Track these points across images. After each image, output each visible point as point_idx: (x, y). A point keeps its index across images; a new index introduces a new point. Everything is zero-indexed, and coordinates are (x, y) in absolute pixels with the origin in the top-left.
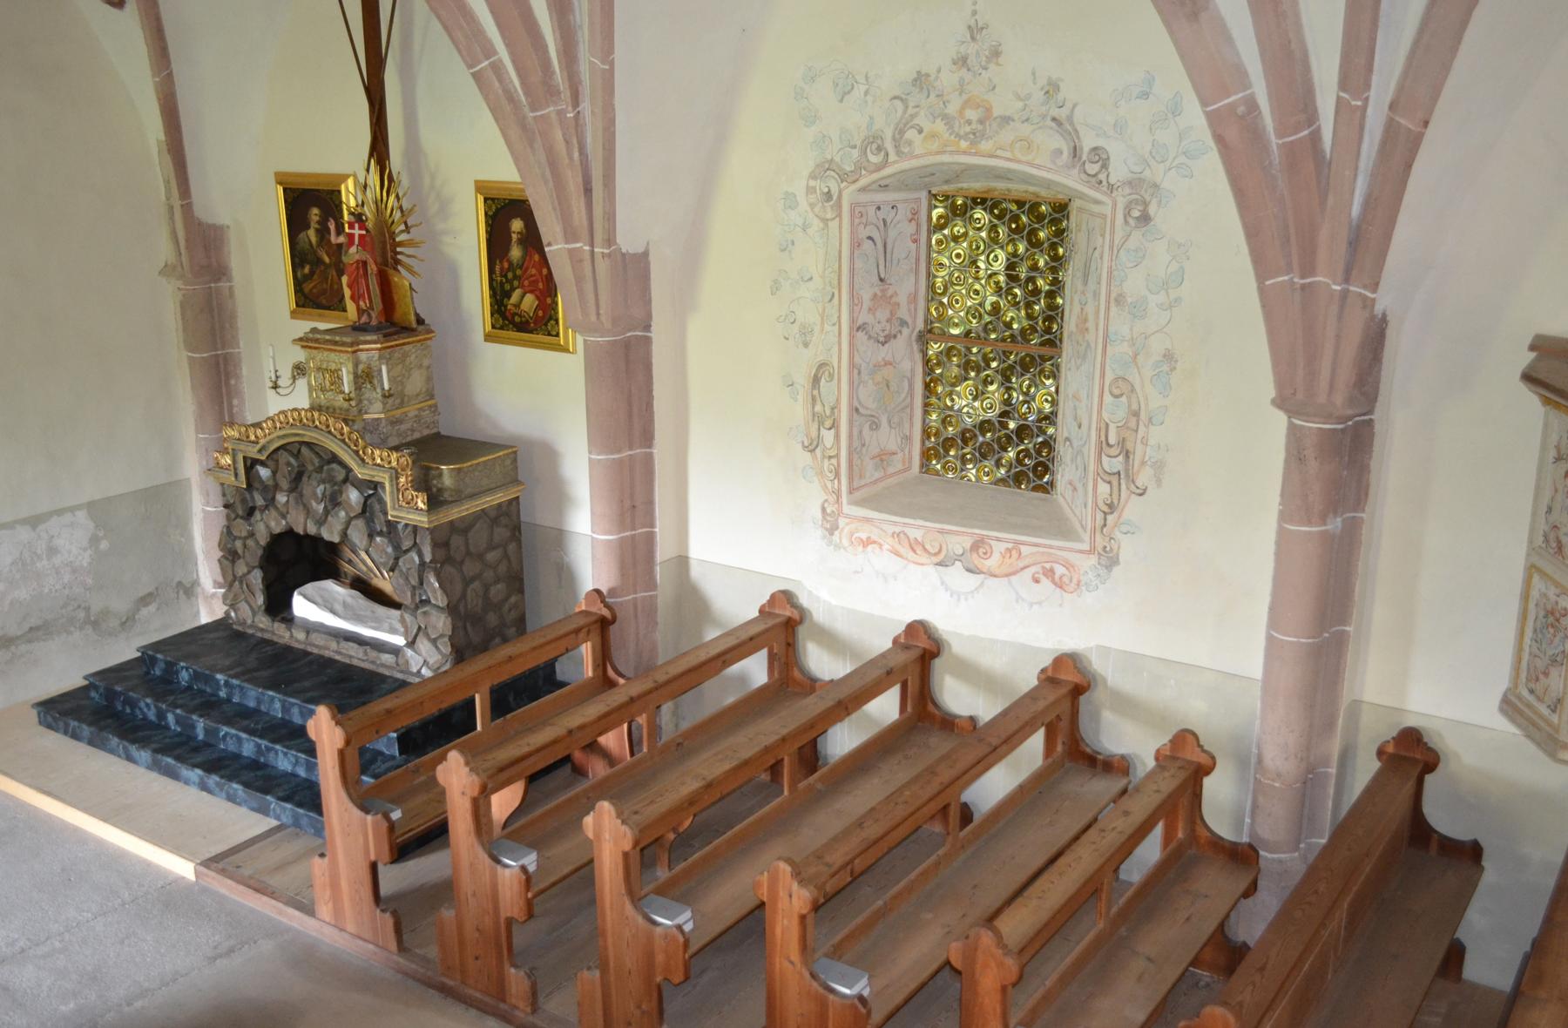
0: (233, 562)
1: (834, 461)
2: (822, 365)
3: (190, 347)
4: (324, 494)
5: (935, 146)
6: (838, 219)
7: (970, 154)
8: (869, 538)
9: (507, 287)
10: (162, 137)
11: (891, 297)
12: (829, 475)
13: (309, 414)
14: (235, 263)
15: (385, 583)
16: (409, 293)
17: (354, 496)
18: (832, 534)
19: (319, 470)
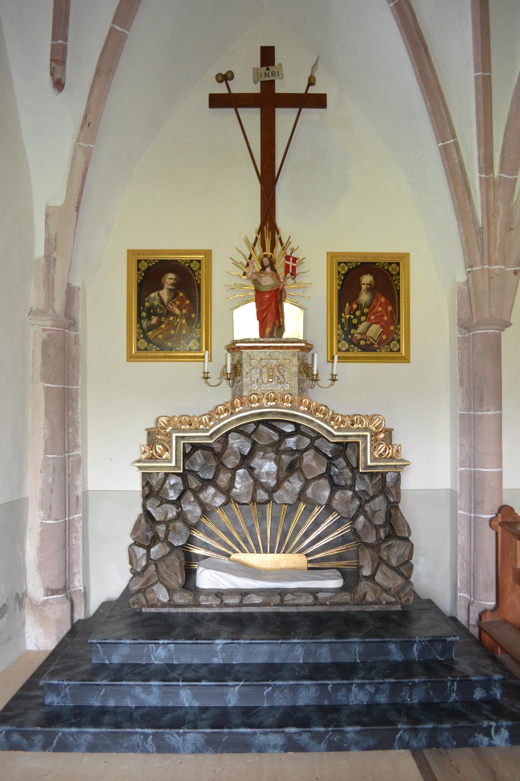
3: (45, 378)
9: (355, 321)
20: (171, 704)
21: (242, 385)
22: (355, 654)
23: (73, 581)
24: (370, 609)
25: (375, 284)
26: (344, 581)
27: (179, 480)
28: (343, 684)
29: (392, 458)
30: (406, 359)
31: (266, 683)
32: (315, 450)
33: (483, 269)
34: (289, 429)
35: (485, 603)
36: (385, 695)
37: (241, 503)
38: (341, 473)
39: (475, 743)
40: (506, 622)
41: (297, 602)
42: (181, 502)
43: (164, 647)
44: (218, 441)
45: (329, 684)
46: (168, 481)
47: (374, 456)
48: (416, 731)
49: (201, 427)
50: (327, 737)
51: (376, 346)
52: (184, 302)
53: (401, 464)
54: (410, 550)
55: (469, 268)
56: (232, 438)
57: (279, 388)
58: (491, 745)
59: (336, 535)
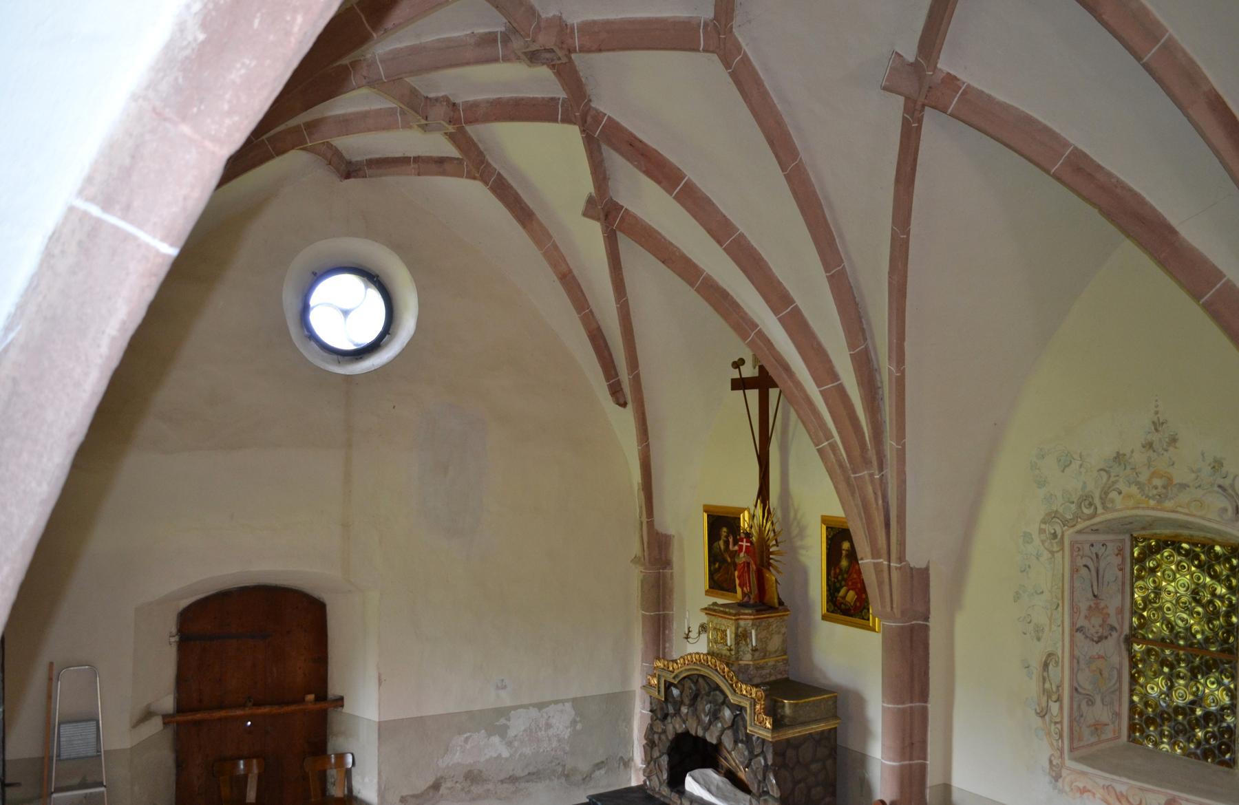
0: (652, 748)
1: (1059, 726)
2: (1050, 655)
4: (709, 710)
5: (1131, 503)
6: (1061, 552)
7: (1157, 510)
8: (1084, 787)
9: (838, 585)
10: (640, 481)
11: (1103, 609)
12: (1055, 735)
13: (705, 657)
14: (675, 559)
15: (743, 774)
16: (774, 585)
17: (727, 713)
18: (1057, 781)
19: (708, 694)
51: (852, 611)
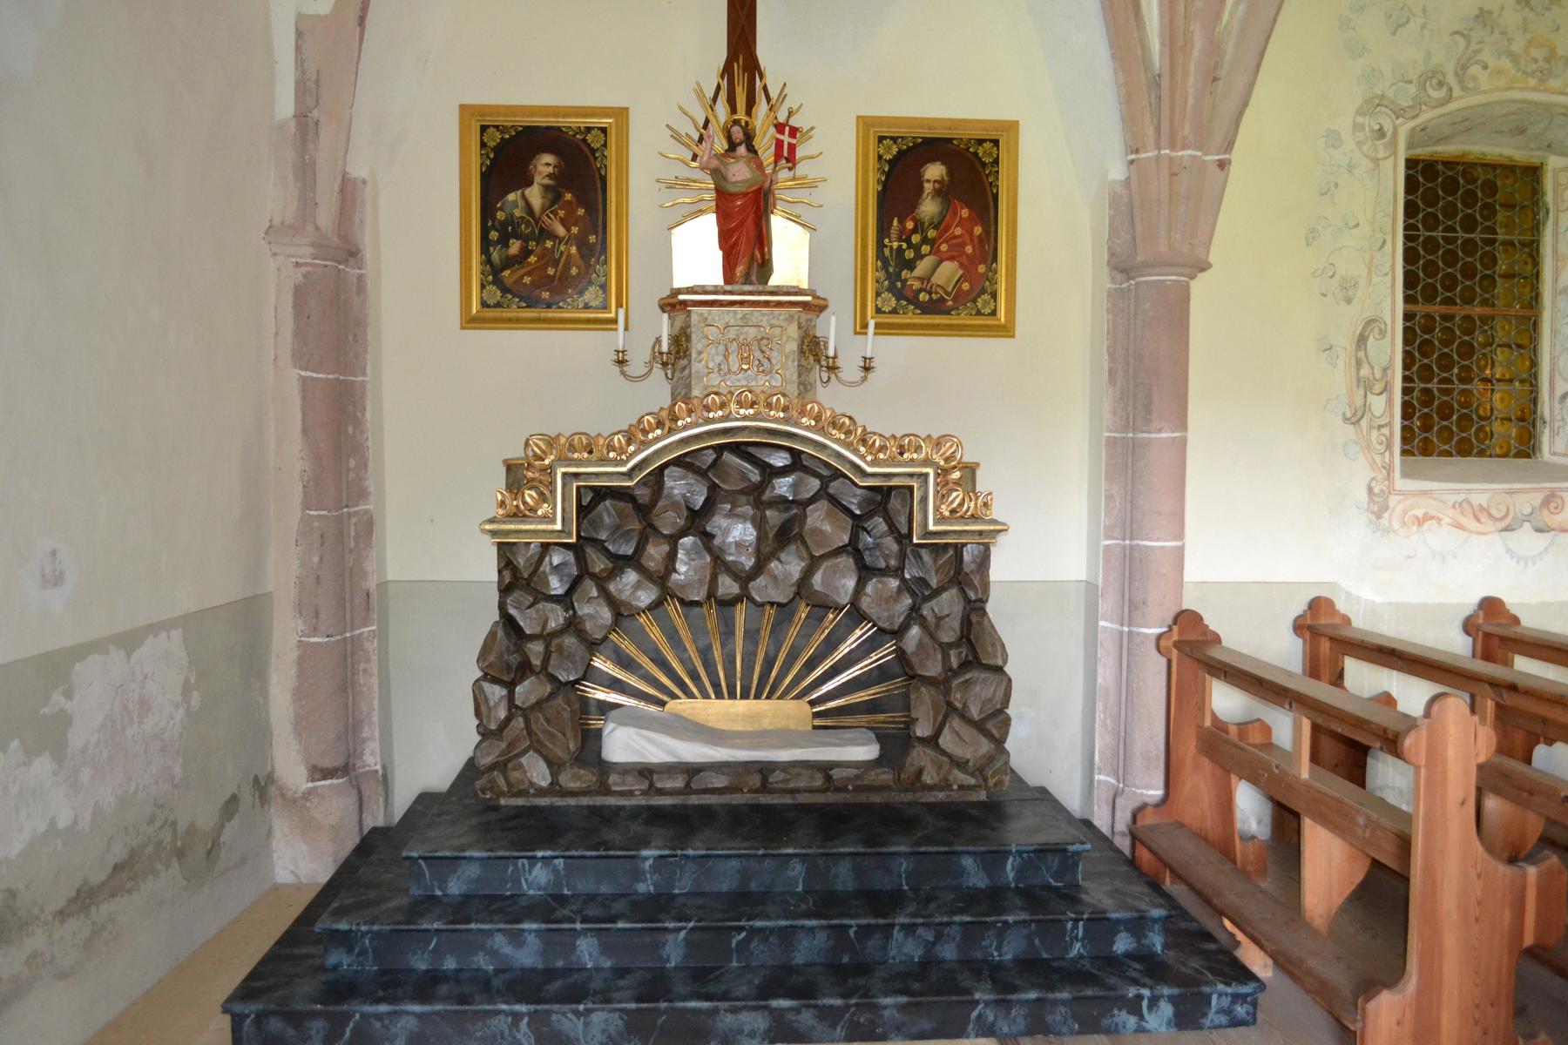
9: (910, 254)
20: (560, 964)
21: (690, 376)
22: (901, 876)
23: (362, 754)
24: (929, 798)
25: (951, 181)
26: (881, 749)
27: (570, 557)
28: (877, 926)
29: (974, 518)
30: (1006, 331)
31: (737, 923)
32: (830, 501)
33: (1158, 158)
34: (779, 460)
35: (1144, 792)
36: (953, 945)
37: (686, 599)
38: (878, 545)
39: (1113, 1026)
40: (1181, 825)
41: (791, 785)
42: (574, 599)
43: (545, 864)
44: (642, 482)
45: (851, 926)
46: (547, 559)
47: (941, 513)
48: (1004, 1005)
49: (612, 455)
50: (847, 1015)
51: (950, 303)
52: (574, 212)
53: (992, 528)
54: (1006, 689)
55: (1132, 153)
56: (670, 477)
57: (761, 383)
58: (1141, 1030)
59: (866, 666)
